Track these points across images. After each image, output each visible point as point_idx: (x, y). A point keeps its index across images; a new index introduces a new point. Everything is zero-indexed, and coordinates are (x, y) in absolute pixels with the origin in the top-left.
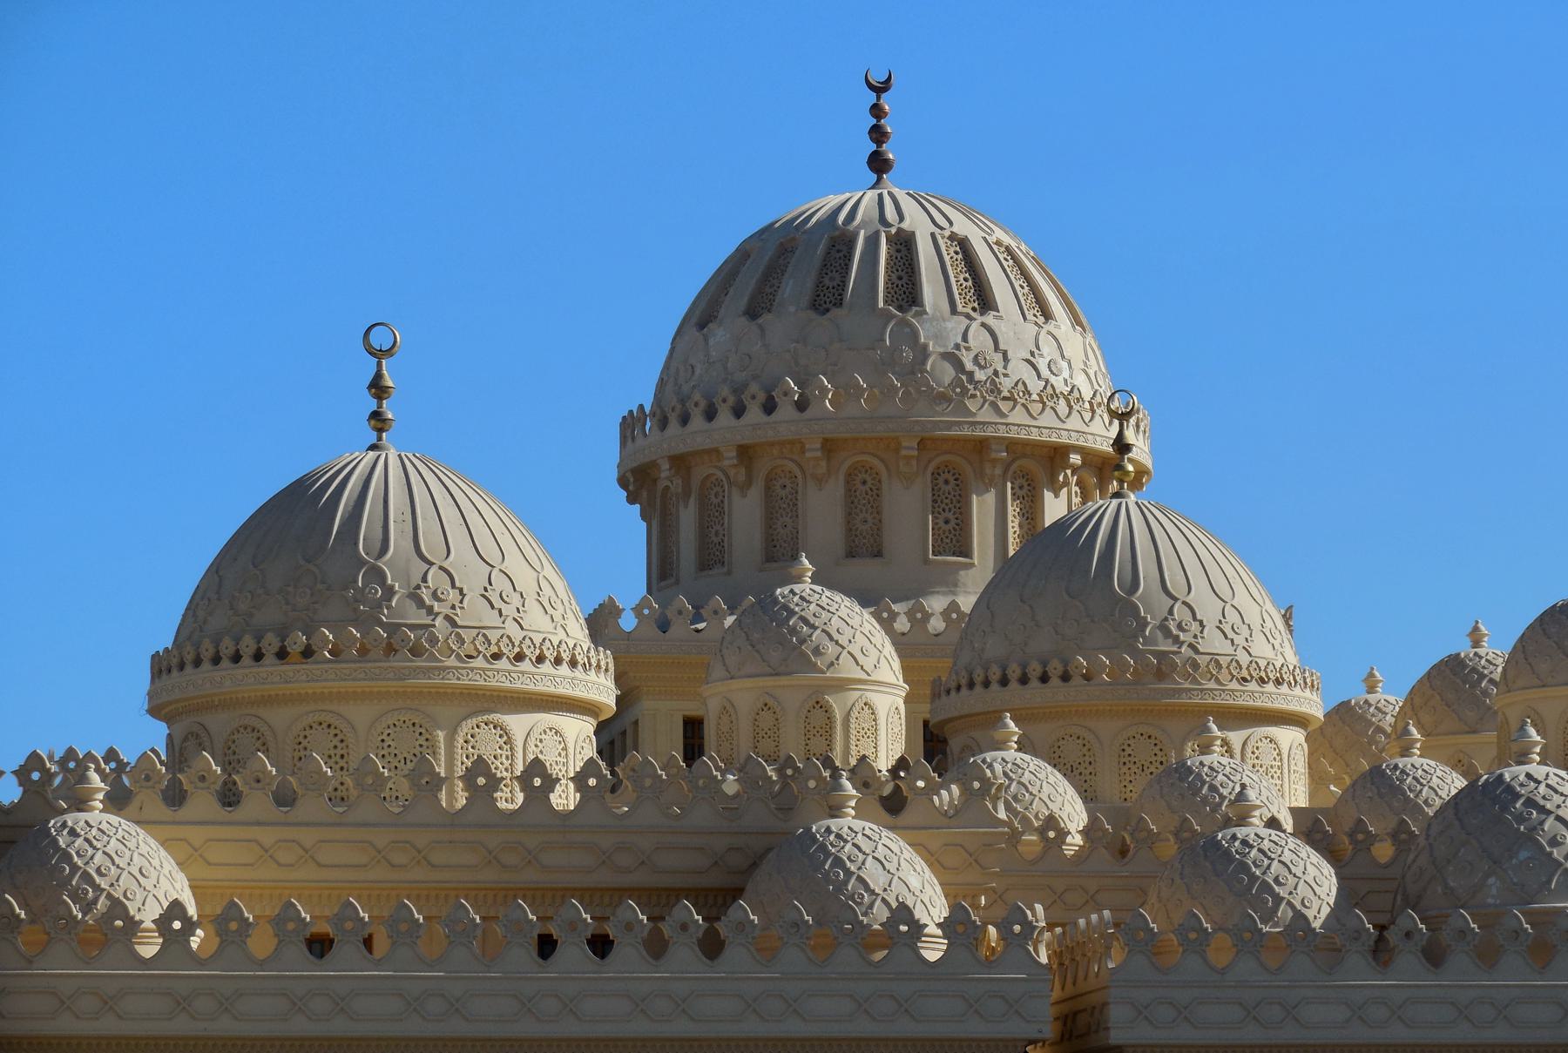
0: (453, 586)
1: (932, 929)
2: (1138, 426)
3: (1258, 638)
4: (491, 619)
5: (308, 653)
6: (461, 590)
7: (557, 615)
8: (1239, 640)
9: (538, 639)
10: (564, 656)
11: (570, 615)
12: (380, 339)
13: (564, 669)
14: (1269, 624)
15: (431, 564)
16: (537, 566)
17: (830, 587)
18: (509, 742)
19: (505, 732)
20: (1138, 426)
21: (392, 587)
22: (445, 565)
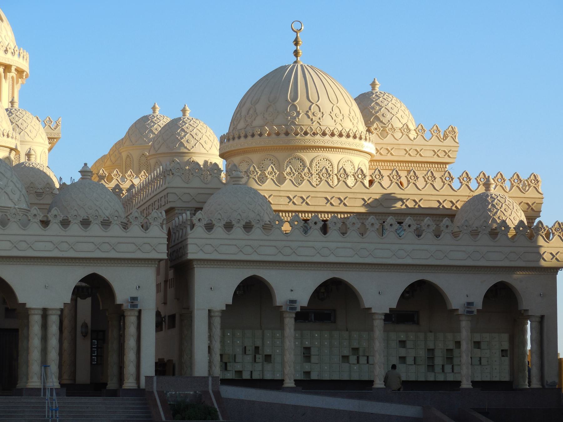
0: (320, 111)
1: (512, 229)
2: (23, 57)
3: (327, 117)
4: (308, 122)
5: (261, 135)
6: (323, 113)
7: (355, 123)
8: (338, 120)
9: (347, 130)
10: (351, 134)
11: (360, 122)
12: (296, 26)
13: (351, 139)
14: (353, 114)
15: (313, 103)
16: (350, 105)
17: (408, 108)
18: (332, 165)
19: (302, 161)
20: (23, 57)
21: (299, 112)
22: (317, 103)
